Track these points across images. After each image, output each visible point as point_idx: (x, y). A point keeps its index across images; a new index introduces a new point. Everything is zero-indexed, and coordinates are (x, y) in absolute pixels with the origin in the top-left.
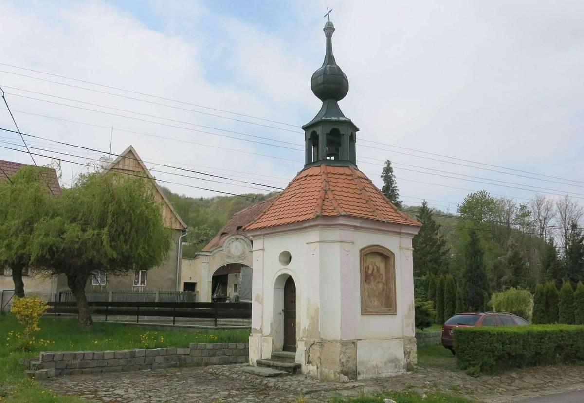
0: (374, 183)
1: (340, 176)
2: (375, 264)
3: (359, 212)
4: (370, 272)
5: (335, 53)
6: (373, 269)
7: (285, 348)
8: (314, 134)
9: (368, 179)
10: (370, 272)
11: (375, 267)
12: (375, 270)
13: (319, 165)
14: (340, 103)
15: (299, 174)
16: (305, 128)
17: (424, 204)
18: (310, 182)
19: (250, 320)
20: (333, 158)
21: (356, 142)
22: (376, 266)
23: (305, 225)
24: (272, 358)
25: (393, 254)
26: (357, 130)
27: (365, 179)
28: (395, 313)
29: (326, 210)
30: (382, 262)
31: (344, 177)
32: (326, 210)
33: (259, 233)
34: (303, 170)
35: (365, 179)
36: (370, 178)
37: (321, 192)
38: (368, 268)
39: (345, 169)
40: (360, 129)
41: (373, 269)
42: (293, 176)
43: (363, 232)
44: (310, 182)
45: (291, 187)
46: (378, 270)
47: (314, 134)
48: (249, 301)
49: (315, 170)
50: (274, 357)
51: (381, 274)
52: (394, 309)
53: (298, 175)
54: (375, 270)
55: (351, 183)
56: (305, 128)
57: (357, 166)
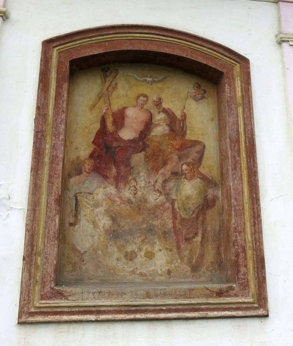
2: (158, 103)
6: (148, 125)
41: (148, 125)
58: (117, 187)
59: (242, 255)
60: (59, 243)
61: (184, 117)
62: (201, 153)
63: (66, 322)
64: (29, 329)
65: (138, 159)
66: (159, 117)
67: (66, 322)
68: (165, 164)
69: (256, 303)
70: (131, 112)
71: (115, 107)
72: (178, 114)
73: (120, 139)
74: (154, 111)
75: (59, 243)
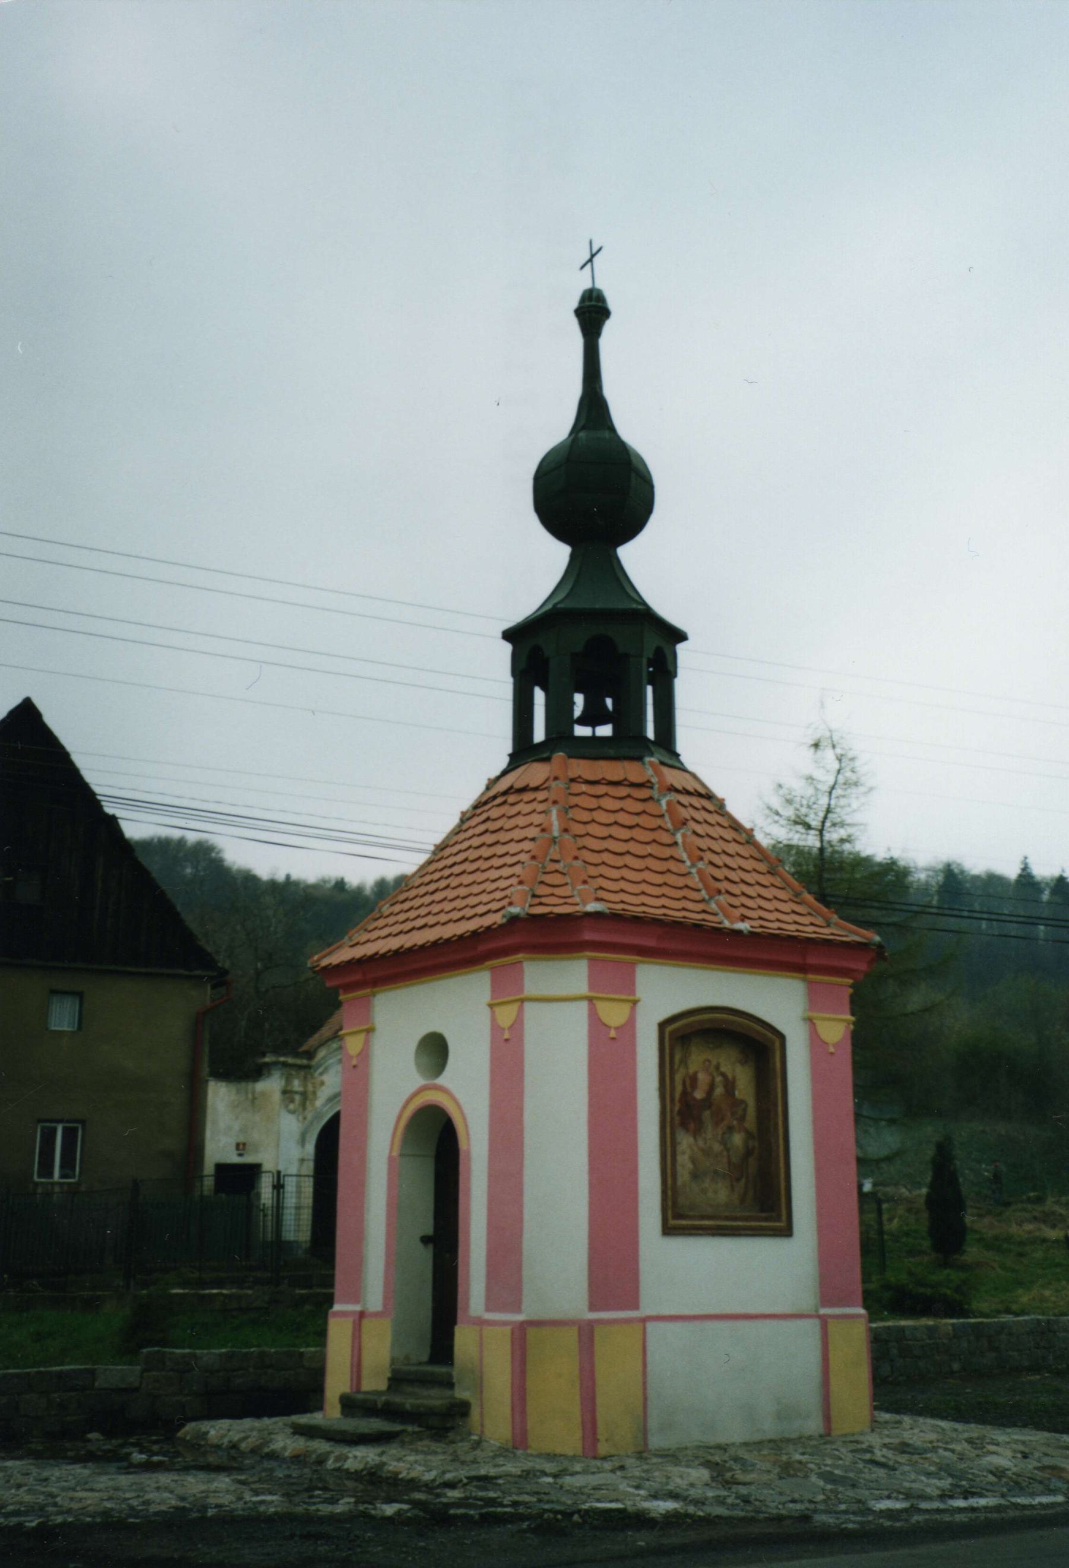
0: (731, 808)
1: (611, 790)
2: (717, 1067)
3: (678, 905)
4: (699, 1095)
5: (611, 390)
6: (712, 1087)
7: (434, 1359)
8: (536, 652)
9: (709, 796)
10: (699, 1095)
11: (719, 1079)
12: (719, 1091)
13: (545, 755)
14: (629, 554)
15: (492, 783)
16: (509, 635)
17: (1025, 868)
18: (514, 810)
19: (331, 1291)
20: (605, 731)
21: (675, 675)
22: (723, 1075)
23: (482, 948)
24: (389, 1387)
25: (782, 1037)
26: (680, 636)
27: (700, 795)
28: (786, 1231)
29: (543, 900)
30: (743, 1062)
31: (623, 791)
32: (543, 900)
33: (357, 977)
34: (504, 773)
35: (700, 795)
36: (719, 791)
37: (538, 842)
38: (694, 1079)
39: (626, 764)
40: (690, 635)
41: (712, 1087)
42: (472, 791)
43: (787, 977)
44: (514, 810)
45: (464, 827)
46: (730, 1086)
47: (536, 652)
48: (331, 1291)
49: (535, 773)
50: (398, 1380)
51: (742, 1102)
52: (784, 1217)
53: (488, 788)
54: (719, 1091)
55: (644, 812)
56: (509, 635)
57: (677, 755)
58: (695, 1138)
59: (988, 1171)
60: (917, 905)
61: (734, 1078)
62: (745, 1110)
63: (162, 815)
64: (531, 822)
65: (707, 1114)
66: (719, 1079)
67: (162, 815)
68: (723, 1119)
69: (244, 1500)
70: (701, 1076)
71: (691, 1071)
72: (730, 1076)
73: (695, 1099)
74: (715, 1074)
75: (917, 905)
